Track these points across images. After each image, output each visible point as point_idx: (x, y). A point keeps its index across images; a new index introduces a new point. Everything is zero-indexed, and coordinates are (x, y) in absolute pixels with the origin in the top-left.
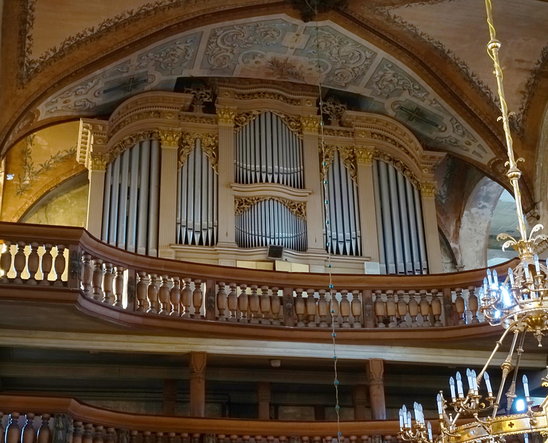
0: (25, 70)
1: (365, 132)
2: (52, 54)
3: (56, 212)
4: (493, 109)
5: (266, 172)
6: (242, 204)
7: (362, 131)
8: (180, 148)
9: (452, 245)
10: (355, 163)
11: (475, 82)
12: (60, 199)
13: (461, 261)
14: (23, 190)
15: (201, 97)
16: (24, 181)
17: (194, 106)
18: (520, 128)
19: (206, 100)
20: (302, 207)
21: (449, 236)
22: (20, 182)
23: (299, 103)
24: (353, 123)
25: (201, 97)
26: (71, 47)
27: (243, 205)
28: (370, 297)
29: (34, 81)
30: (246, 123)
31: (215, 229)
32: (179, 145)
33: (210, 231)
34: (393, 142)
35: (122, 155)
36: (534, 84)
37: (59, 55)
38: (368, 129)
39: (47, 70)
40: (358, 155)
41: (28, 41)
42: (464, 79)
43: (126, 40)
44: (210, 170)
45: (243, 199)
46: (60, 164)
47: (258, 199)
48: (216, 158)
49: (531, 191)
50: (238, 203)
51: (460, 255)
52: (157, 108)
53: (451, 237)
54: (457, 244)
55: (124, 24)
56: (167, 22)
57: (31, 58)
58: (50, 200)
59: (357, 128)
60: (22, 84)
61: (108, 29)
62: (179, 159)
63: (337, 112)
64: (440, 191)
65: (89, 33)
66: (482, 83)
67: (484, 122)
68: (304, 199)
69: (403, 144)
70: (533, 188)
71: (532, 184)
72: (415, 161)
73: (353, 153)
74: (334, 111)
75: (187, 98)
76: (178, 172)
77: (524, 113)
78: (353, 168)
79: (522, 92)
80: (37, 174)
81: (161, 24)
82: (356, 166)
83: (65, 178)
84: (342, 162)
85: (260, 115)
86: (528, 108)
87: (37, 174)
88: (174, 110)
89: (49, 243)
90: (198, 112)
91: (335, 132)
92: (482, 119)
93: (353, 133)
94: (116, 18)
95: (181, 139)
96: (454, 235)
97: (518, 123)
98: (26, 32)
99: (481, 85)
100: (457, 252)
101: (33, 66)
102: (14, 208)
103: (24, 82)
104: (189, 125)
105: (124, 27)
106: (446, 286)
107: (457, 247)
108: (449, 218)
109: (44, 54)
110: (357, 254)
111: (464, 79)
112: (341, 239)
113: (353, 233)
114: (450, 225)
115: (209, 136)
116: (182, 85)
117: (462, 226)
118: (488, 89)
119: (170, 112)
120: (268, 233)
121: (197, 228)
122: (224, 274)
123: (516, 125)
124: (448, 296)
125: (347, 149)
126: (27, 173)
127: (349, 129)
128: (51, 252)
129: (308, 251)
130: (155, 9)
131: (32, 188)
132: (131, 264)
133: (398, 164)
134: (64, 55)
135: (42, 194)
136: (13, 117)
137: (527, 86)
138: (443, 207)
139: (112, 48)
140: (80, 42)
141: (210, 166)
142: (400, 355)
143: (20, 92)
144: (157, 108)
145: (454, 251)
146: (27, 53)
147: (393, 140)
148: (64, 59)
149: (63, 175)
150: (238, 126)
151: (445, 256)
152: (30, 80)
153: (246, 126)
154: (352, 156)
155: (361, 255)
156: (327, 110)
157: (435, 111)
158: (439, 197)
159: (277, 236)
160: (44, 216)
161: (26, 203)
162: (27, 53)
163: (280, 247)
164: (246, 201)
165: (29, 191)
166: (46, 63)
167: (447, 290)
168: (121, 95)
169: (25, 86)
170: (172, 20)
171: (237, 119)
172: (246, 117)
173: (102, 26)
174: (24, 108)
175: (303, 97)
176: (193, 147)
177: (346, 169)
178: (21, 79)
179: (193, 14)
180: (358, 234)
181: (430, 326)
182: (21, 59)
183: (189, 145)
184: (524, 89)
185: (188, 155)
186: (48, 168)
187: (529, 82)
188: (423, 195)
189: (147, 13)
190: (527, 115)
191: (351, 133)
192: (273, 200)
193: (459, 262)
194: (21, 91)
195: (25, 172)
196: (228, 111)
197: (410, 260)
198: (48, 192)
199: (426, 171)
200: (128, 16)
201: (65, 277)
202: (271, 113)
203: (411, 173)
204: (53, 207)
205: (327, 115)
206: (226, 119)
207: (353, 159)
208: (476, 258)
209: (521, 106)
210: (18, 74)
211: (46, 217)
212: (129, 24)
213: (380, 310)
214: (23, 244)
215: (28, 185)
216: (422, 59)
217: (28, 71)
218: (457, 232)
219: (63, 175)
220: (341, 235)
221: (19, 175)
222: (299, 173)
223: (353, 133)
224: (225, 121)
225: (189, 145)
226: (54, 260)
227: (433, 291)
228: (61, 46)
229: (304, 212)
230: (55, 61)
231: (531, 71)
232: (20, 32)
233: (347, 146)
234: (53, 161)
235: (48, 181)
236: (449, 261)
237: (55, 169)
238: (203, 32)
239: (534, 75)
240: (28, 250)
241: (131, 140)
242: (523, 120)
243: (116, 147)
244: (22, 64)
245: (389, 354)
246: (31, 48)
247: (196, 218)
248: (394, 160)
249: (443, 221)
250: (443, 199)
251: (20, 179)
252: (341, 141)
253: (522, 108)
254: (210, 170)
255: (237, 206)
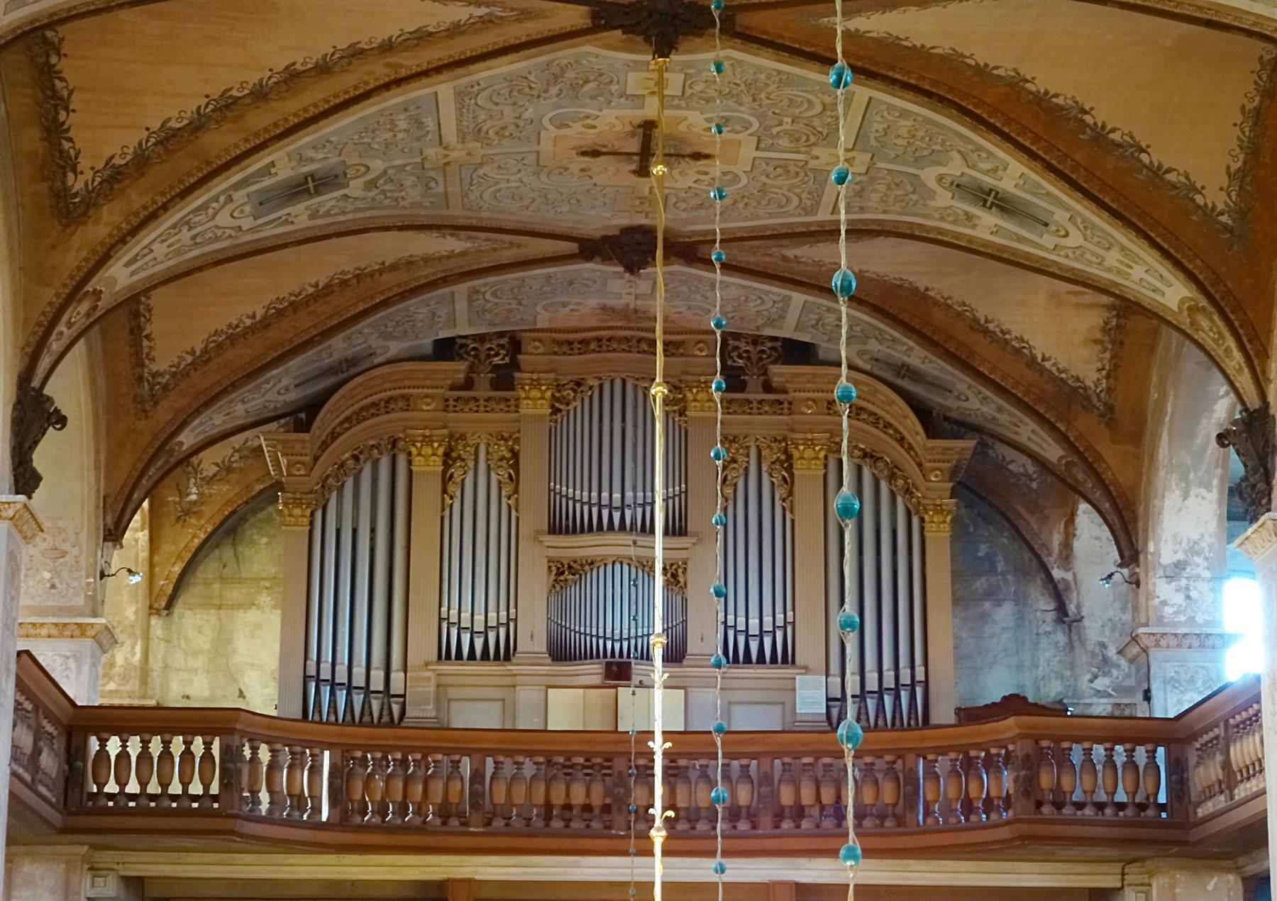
0: (147, 388)
1: (814, 400)
2: (189, 359)
3: (253, 543)
4: (1041, 375)
5: (610, 507)
6: (563, 573)
7: (808, 399)
8: (447, 466)
9: (1057, 573)
10: (790, 469)
11: (994, 332)
12: (261, 515)
13: (1078, 607)
14: (187, 512)
15: (488, 356)
16: (188, 495)
17: (474, 375)
18: (1105, 404)
19: (496, 360)
20: (680, 571)
21: (1050, 555)
22: (181, 498)
23: (681, 351)
24: (788, 385)
25: (488, 356)
26: (220, 346)
27: (565, 574)
28: (769, 770)
29: (164, 404)
30: (574, 404)
31: (512, 625)
32: (445, 463)
33: (502, 631)
34: (871, 419)
35: (341, 490)
36: (1118, 327)
37: (202, 360)
38: (820, 394)
39: (183, 385)
40: (796, 454)
41: (145, 343)
42: (971, 328)
43: (315, 326)
44: (504, 506)
45: (565, 562)
46: (250, 462)
47: (592, 563)
48: (515, 480)
49: (1130, 527)
50: (554, 572)
51: (1075, 594)
52: (403, 391)
53: (1055, 556)
54: (1068, 570)
55: (307, 303)
56: (381, 293)
57: (154, 368)
58: (243, 520)
59: (797, 394)
60: (144, 411)
61: (280, 313)
62: (444, 491)
63: (761, 359)
64: (1024, 466)
65: (249, 322)
66: (1009, 332)
67: (1026, 399)
68: (683, 554)
69: (892, 421)
70: (1135, 520)
71: (1133, 511)
72: (915, 457)
73: (786, 452)
74: (754, 358)
75: (457, 369)
76: (442, 518)
77: (1108, 377)
78: (786, 481)
79: (1096, 342)
80: (210, 481)
81: (373, 297)
82: (792, 475)
83: (262, 487)
84: (764, 468)
85: (601, 386)
86: (1116, 367)
87: (210, 481)
88: (435, 391)
89: (189, 733)
90: (482, 391)
91: (755, 405)
92: (1020, 395)
93: (790, 403)
94: (291, 294)
95: (446, 455)
96: (1061, 552)
97: (1098, 396)
98: (141, 329)
99: (1007, 336)
100: (1068, 588)
101: (159, 380)
102: (173, 547)
103: (147, 407)
104: (465, 420)
105: (308, 306)
106: (909, 750)
107: (1069, 576)
108: (1048, 518)
109: (176, 360)
110: (785, 661)
111: (971, 328)
112: (754, 630)
113: (780, 617)
114: (1051, 533)
115: (503, 438)
116: (446, 349)
117: (1078, 532)
118: (1023, 341)
119: (427, 396)
120: (609, 631)
121: (479, 627)
122: (503, 742)
123: (1095, 400)
124: (911, 769)
125: (776, 440)
126: (193, 480)
127: (781, 397)
128: (192, 748)
129: (685, 662)
130: (357, 276)
131: (203, 508)
132: (335, 740)
133: (880, 464)
134: (209, 360)
135: (222, 518)
136: (134, 468)
137: (1104, 330)
138: (1034, 496)
139: (291, 341)
140: (234, 337)
141: (504, 500)
142: (827, 873)
143: (142, 424)
144: (403, 391)
145: (1061, 587)
146: (147, 362)
147: (872, 414)
148: (210, 365)
149: (257, 480)
150: (560, 410)
151: (1043, 595)
152: (156, 404)
153: (575, 408)
154: (783, 457)
155: (793, 662)
156: (740, 357)
157: (936, 373)
158: (1023, 478)
159: (625, 636)
160: (232, 553)
161: (195, 536)
162: (147, 362)
163: (619, 664)
164: (570, 567)
165: (199, 514)
166: (180, 375)
167: (910, 757)
168: (332, 380)
169: (150, 414)
170: (390, 289)
171: (557, 395)
172: (575, 391)
173: (268, 309)
174: (151, 451)
175: (689, 336)
176: (471, 464)
177: (773, 483)
178: (142, 402)
179: (426, 276)
180: (790, 619)
181: (877, 826)
182: (137, 371)
183: (463, 460)
184: (1099, 336)
185: (463, 480)
186: (229, 470)
187: (1106, 323)
188: (928, 527)
189: (344, 283)
190: (1116, 380)
191: (786, 405)
192: (622, 563)
193: (1072, 608)
194: (144, 422)
195: (188, 480)
196: (536, 384)
197: (892, 667)
198: (232, 514)
199: (936, 476)
200: (311, 290)
201: (215, 789)
202: (624, 381)
203: (906, 483)
204: (248, 533)
205: (741, 368)
206: (534, 399)
207: (787, 462)
208: (1111, 598)
209: (1099, 365)
210: (135, 396)
211: (235, 555)
212: (316, 301)
213: (786, 797)
214: (147, 737)
215: (195, 503)
216: (878, 303)
217: (151, 389)
218: (1067, 546)
219: (257, 480)
220: (754, 622)
221: (178, 485)
222: (677, 499)
223: (790, 403)
224: (534, 404)
225: (463, 460)
226: (197, 760)
227: (888, 758)
228: (202, 346)
229: (682, 580)
230: (195, 370)
231: (1104, 306)
232: (131, 331)
233: (775, 433)
234: (237, 456)
235: (232, 494)
236: (1052, 606)
237: (241, 470)
238: (453, 293)
239: (1114, 313)
240: (156, 747)
241: (356, 458)
242: (1109, 390)
243: (327, 477)
244: (140, 379)
245: (807, 872)
246: (153, 353)
247: (474, 610)
248: (872, 456)
249: (1035, 527)
250: (1032, 480)
251: (180, 492)
252: (766, 424)
253: (1103, 369)
254: (504, 506)
255: (553, 577)
